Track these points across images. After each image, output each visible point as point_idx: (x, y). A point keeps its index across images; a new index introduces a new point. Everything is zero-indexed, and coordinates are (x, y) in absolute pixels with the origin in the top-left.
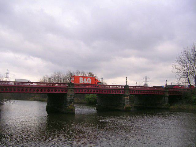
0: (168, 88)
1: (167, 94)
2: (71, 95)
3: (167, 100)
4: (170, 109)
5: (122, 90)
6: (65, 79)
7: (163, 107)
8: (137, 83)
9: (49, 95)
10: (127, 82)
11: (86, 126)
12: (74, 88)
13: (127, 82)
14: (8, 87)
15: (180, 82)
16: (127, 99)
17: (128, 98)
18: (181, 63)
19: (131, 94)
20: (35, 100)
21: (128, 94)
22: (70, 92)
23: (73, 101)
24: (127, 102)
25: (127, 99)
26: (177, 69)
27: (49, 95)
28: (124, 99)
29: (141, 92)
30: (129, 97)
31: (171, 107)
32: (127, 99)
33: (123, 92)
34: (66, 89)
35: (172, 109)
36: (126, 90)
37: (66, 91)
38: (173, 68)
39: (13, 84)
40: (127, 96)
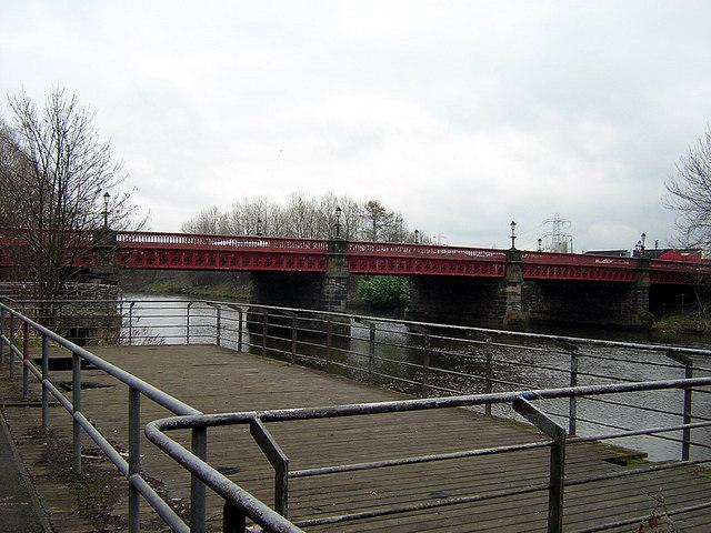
0: (644, 258)
1: (646, 282)
2: (338, 279)
3: (644, 299)
4: (653, 330)
5: (499, 263)
6: (281, 220)
7: (629, 323)
8: (513, 224)
9: (257, 276)
10: (513, 238)
11: (703, 315)
12: (348, 257)
13: (513, 238)
14: (142, 250)
15: (691, 241)
16: (513, 292)
17: (518, 289)
18: (697, 176)
19: (525, 279)
20: (171, 292)
21: (516, 277)
22: (334, 269)
23: (345, 298)
24: (513, 304)
25: (513, 292)
26: (682, 196)
27: (257, 276)
28: (505, 293)
29: (559, 273)
30: (519, 286)
31: (656, 325)
32: (514, 294)
33: (500, 271)
34: (322, 258)
35: (659, 330)
36: (511, 264)
37: (322, 264)
38: (669, 193)
39: (180, 240)
40: (514, 284)
